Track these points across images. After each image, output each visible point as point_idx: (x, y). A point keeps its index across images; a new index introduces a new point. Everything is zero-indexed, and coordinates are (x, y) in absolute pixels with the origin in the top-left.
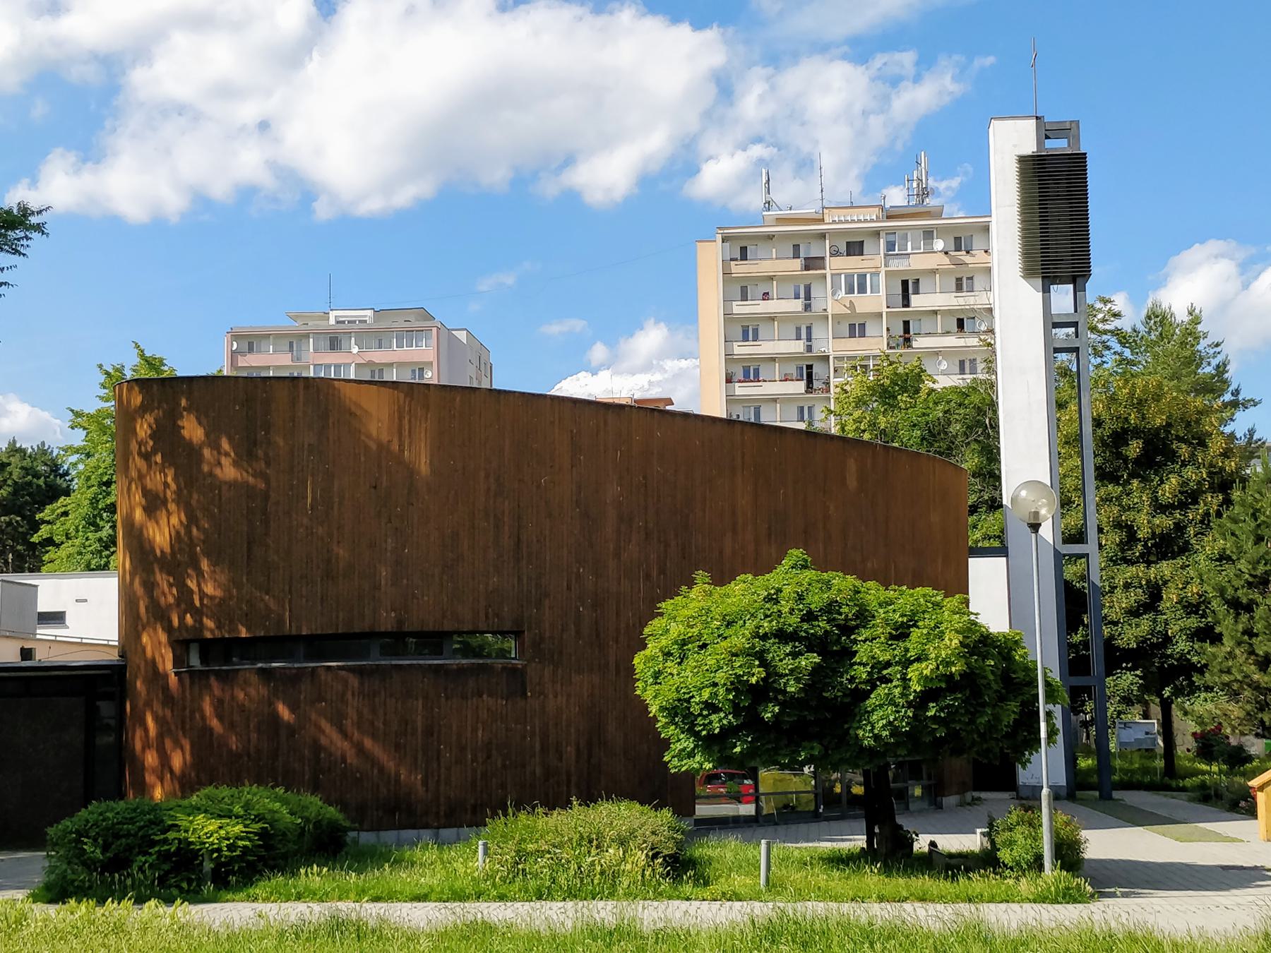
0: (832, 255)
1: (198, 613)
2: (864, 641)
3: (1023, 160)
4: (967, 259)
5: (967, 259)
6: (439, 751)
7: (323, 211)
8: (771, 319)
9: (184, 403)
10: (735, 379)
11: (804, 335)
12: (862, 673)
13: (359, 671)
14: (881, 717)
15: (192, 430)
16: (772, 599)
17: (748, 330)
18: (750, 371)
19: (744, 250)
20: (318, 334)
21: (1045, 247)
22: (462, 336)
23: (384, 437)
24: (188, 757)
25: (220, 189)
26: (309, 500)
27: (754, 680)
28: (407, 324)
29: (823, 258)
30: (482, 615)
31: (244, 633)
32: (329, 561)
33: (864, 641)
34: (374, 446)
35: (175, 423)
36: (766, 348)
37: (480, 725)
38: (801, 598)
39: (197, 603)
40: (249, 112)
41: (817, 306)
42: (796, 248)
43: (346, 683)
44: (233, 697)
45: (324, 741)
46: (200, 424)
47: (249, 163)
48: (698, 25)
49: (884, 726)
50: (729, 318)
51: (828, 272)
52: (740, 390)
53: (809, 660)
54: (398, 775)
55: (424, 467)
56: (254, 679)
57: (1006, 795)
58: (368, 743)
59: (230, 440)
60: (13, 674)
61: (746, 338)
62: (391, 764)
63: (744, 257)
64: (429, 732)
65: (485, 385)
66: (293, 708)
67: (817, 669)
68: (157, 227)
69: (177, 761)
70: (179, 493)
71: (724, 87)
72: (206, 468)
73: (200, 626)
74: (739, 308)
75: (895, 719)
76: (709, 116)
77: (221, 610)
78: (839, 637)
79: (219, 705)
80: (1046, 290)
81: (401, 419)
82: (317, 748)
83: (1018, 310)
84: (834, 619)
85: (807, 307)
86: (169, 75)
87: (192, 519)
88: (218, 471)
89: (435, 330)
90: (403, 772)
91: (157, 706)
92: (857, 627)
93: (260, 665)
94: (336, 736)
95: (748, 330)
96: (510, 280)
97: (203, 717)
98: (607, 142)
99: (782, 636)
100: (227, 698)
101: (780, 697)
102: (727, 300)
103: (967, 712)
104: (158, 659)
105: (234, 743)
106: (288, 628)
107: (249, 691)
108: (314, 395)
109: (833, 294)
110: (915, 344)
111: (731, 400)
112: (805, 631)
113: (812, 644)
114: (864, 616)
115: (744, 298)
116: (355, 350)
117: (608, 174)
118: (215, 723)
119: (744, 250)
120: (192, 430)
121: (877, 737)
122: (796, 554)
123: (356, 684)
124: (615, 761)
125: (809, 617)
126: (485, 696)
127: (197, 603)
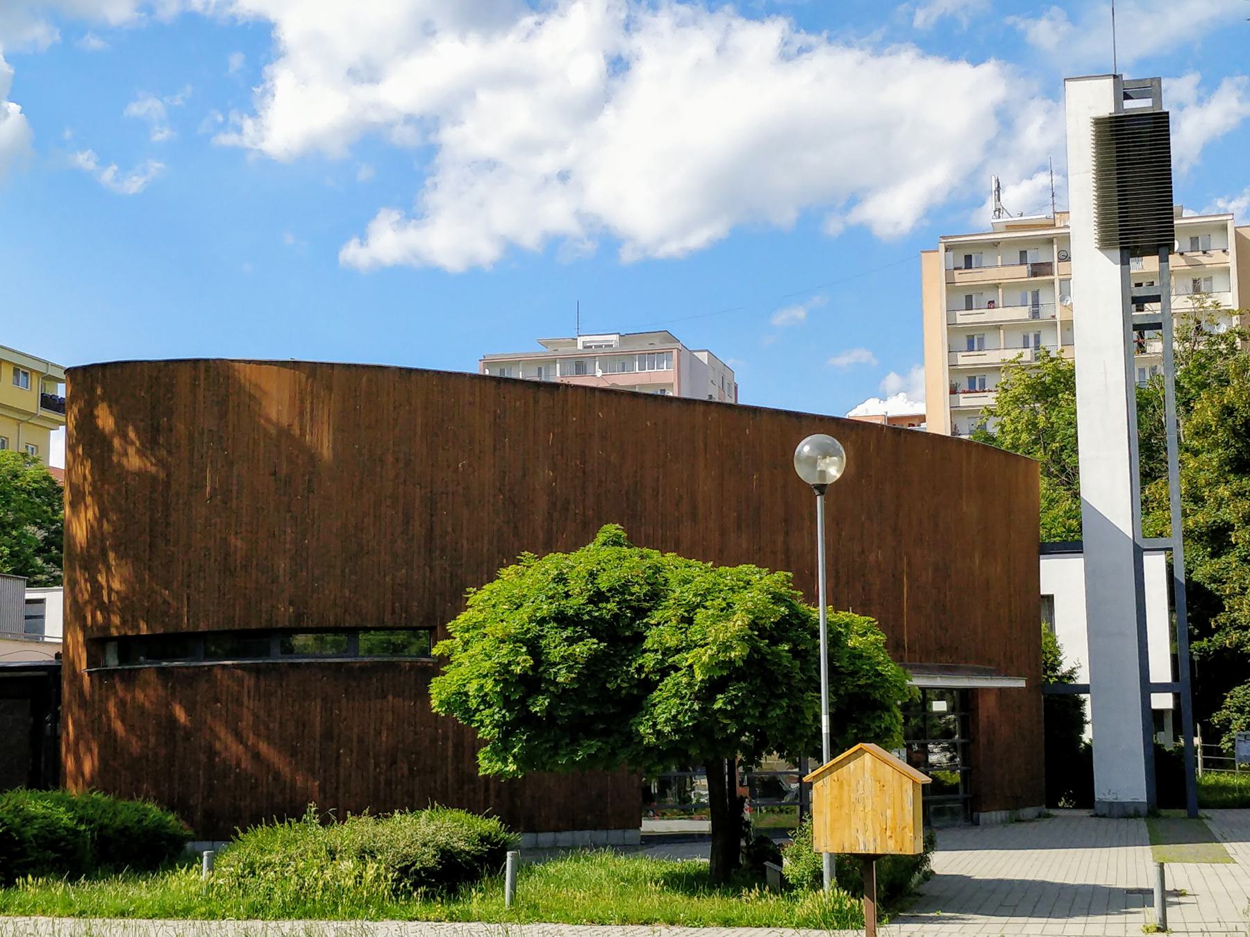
0: (1060, 260)
1: (106, 609)
2: (658, 624)
3: (1099, 122)
4: (1204, 259)
5: (1204, 259)
6: (338, 756)
7: (627, 255)
8: (997, 327)
9: (99, 391)
10: (959, 390)
11: (1032, 343)
12: (649, 660)
13: (256, 670)
14: (666, 710)
15: (105, 420)
16: (561, 579)
17: (973, 339)
18: (973, 381)
19: (968, 259)
20: (564, 360)
21: (1123, 215)
22: (704, 357)
23: (285, 422)
24: (96, 763)
25: (530, 239)
26: (208, 489)
27: (518, 670)
28: (651, 347)
29: (1050, 264)
30: (389, 609)
31: (144, 630)
32: (227, 555)
33: (658, 624)
34: (273, 431)
35: (91, 413)
36: (992, 357)
37: (384, 728)
38: (593, 575)
39: (106, 599)
40: (547, 163)
41: (1045, 313)
42: (1023, 254)
43: (240, 682)
44: (134, 698)
45: (218, 746)
46: (111, 413)
47: (557, 214)
48: (976, 61)
49: (667, 720)
50: (952, 328)
51: (1056, 277)
52: (965, 401)
53: (585, 648)
54: (293, 780)
55: (326, 452)
56: (153, 677)
57: (1084, 813)
58: (263, 747)
59: (137, 430)
60: (6, 674)
61: (971, 348)
62: (287, 769)
63: (968, 265)
64: (328, 736)
65: (730, 400)
66: (189, 711)
67: (594, 659)
68: (474, 275)
69: (87, 768)
70: (93, 484)
71: (1005, 120)
72: (115, 459)
73: (107, 624)
74: (963, 318)
75: (678, 713)
76: (990, 148)
77: (128, 607)
78: (633, 620)
79: (122, 704)
80: (1124, 262)
81: (302, 401)
82: (211, 753)
83: (1095, 282)
84: (625, 600)
85: (1035, 315)
86: (470, 137)
87: (103, 515)
88: (125, 461)
89: (675, 352)
90: (299, 779)
91: (75, 709)
92: (650, 610)
93: (164, 664)
94: (230, 740)
95: (973, 339)
96: (801, 314)
97: (109, 718)
98: (891, 177)
99: (561, 619)
100: (129, 698)
101: (552, 689)
102: (951, 310)
103: (756, 705)
104: (77, 661)
105: (135, 746)
106: (185, 625)
107: (147, 695)
108: (212, 378)
109: (1062, 300)
110: (1149, 349)
111: (955, 412)
112: (589, 613)
113: (598, 628)
114: (656, 596)
115: (969, 307)
116: (599, 373)
117: (896, 208)
118: (118, 726)
119: (968, 259)
120: (105, 420)
121: (659, 734)
122: (611, 529)
123: (252, 682)
124: (425, 768)
125: (598, 597)
126: (390, 698)
127: (106, 599)
